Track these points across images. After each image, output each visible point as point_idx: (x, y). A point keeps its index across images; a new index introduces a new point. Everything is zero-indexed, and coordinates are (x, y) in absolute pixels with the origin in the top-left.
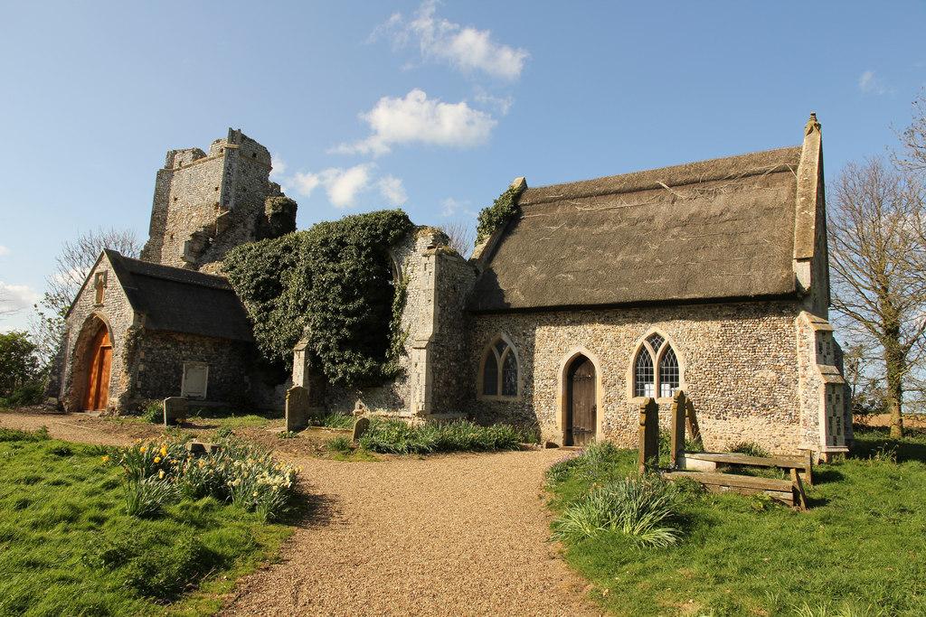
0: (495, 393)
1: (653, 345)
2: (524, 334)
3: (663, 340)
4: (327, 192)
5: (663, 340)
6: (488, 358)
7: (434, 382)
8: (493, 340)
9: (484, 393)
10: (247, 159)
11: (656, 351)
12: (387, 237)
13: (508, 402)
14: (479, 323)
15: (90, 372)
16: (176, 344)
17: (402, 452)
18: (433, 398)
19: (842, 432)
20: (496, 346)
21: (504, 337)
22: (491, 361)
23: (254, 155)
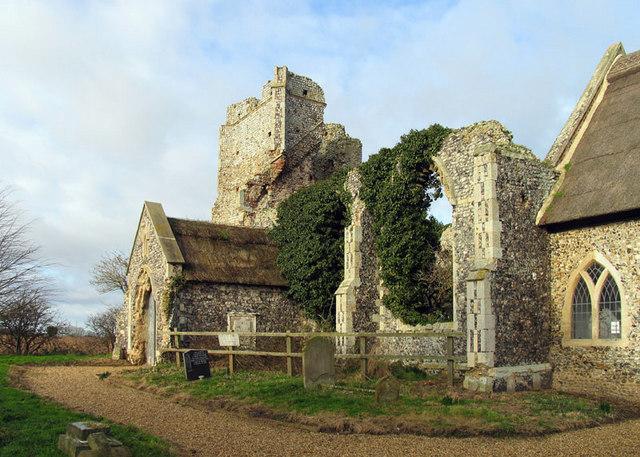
0: (587, 335)
1: (592, 276)
2: (629, 251)
3: (603, 269)
4: (371, 120)
5: (603, 269)
6: (576, 292)
7: (497, 325)
8: (583, 263)
9: (574, 336)
10: (299, 95)
11: (595, 282)
12: (418, 159)
13: (607, 349)
14: (561, 242)
15: (338, 234)
16: (218, 296)
17: (172, 300)
18: (497, 346)
19: (468, 331)
20: (589, 271)
21: (600, 258)
22: (581, 290)
23: (305, 92)
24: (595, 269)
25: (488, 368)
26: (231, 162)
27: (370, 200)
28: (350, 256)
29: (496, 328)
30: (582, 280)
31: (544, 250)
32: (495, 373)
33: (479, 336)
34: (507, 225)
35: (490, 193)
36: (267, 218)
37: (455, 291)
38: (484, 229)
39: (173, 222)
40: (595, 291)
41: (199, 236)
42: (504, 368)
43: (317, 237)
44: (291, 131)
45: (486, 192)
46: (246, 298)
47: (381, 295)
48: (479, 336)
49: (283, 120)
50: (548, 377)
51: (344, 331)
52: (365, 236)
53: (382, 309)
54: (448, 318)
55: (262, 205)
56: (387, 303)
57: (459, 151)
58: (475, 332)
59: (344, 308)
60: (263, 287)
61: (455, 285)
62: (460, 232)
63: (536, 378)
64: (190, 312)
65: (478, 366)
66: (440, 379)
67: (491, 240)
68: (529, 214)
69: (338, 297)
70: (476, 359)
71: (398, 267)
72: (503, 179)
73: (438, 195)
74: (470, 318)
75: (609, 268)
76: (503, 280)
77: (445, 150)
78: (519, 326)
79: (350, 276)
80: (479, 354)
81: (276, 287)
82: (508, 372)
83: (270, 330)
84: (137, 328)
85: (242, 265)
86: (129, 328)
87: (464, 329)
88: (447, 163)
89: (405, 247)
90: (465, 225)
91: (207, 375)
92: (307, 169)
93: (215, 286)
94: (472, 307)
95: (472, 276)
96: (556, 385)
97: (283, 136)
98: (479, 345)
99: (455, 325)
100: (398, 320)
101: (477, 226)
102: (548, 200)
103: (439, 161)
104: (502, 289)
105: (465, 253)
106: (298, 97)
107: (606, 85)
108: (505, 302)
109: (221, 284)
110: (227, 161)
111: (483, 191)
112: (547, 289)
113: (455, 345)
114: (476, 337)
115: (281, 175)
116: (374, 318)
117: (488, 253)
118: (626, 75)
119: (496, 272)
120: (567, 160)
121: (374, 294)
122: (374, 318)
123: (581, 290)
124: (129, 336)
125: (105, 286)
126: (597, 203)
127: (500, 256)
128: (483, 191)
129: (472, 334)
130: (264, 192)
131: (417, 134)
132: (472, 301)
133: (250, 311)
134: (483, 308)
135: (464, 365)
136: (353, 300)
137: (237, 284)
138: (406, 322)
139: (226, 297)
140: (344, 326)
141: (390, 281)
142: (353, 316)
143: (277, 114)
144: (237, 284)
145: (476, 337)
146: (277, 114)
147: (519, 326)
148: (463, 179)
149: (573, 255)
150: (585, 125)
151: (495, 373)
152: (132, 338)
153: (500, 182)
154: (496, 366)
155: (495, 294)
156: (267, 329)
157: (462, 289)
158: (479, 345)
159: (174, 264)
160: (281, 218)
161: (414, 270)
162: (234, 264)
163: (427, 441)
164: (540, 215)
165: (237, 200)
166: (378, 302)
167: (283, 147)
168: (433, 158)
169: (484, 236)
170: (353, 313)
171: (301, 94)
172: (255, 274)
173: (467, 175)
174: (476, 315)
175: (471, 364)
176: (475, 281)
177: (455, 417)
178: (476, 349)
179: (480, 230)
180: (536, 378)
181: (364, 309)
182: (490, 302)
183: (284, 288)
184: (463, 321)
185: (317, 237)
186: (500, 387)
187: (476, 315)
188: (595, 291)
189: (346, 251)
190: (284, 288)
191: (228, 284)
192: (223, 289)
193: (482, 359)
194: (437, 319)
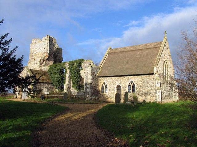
8: (103, 82)
16: (40, 85)
21: (105, 82)
22: (103, 86)
24: (104, 83)
27: (70, 69)
30: (155, 49)
31: (98, 80)
32: (90, 98)
34: (92, 77)
35: (90, 72)
36: (46, 68)
39: (30, 70)
40: (104, 86)
43: (59, 74)
44: (50, 48)
49: (48, 47)
50: (98, 98)
52: (69, 75)
53: (72, 88)
55: (43, 64)
56: (73, 87)
60: (49, 83)
63: (96, 99)
66: (82, 99)
68: (96, 75)
71: (75, 81)
73: (82, 69)
75: (106, 83)
78: (94, 91)
80: (89, 95)
81: (51, 83)
82: (92, 98)
85: (44, 79)
87: (86, 91)
89: (76, 78)
90: (86, 76)
91: (44, 99)
92: (52, 57)
96: (99, 100)
97: (48, 50)
102: (98, 72)
103: (82, 65)
107: (108, 54)
112: (98, 86)
113: (85, 94)
115: (49, 57)
116: (71, 89)
117: (90, 81)
118: (111, 53)
120: (101, 66)
121: (71, 85)
123: (103, 86)
126: (104, 74)
130: (44, 62)
136: (67, 86)
141: (73, 83)
147: (94, 91)
149: (102, 81)
150: (104, 61)
151: (90, 98)
153: (92, 71)
160: (49, 69)
161: (78, 81)
162: (43, 79)
163: (83, 105)
164: (97, 75)
167: (48, 53)
172: (47, 81)
177: (86, 102)
180: (96, 99)
181: (69, 88)
183: (52, 83)
184: (86, 90)
185: (59, 74)
186: (91, 100)
188: (104, 86)
189: (66, 78)
190: (52, 83)
191: (42, 83)
193: (89, 96)
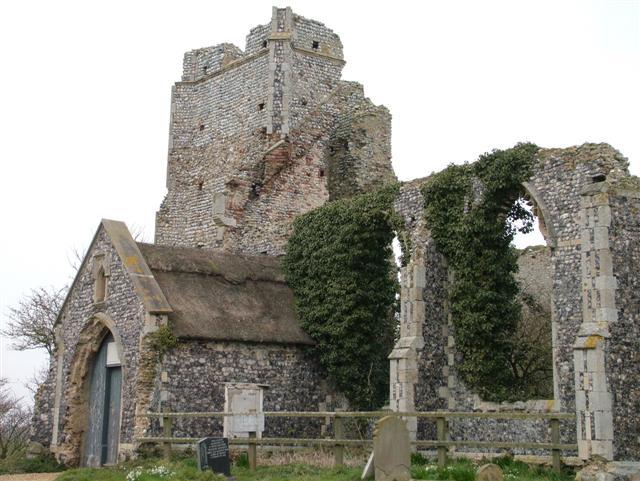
12: (507, 177)
16: (213, 358)
18: (616, 433)
23: (315, 45)
25: (605, 462)
26: (191, 141)
28: (409, 305)
29: (613, 410)
33: (592, 418)
35: (602, 242)
37: (555, 359)
38: (594, 285)
41: (182, 272)
42: (626, 463)
45: (596, 241)
46: (250, 362)
47: (451, 362)
48: (592, 418)
51: (403, 409)
54: (549, 396)
57: (559, 180)
58: (588, 414)
59: (402, 378)
61: (555, 351)
62: (560, 282)
64: (176, 383)
65: (593, 458)
67: (603, 299)
69: (393, 364)
70: (590, 449)
72: (617, 224)
74: (580, 396)
76: (620, 349)
77: (540, 176)
79: (408, 338)
83: (281, 409)
84: (72, 410)
86: (56, 411)
87: (571, 410)
88: (542, 194)
92: (316, 161)
93: (209, 345)
94: (582, 382)
95: (580, 342)
98: (593, 431)
99: (556, 405)
100: (476, 397)
101: (586, 282)
104: (619, 360)
105: (568, 309)
106: (306, 53)
108: (623, 377)
109: (217, 341)
110: (184, 139)
111: (592, 239)
114: (588, 420)
119: (610, 339)
121: (441, 359)
122: (442, 392)
124: (56, 422)
125: (22, 340)
127: (615, 319)
128: (592, 239)
129: (584, 416)
131: (498, 154)
132: (582, 374)
133: (253, 381)
134: (595, 383)
135: (571, 458)
136: (415, 367)
137: (239, 342)
138: (485, 399)
139: (223, 361)
140: (402, 403)
142: (415, 389)
143: (276, 81)
144: (239, 342)
145: (588, 420)
146: (276, 81)
148: (565, 215)
152: (62, 427)
153: (614, 229)
154: (617, 458)
155: (611, 366)
156: (278, 407)
157: (566, 356)
158: (583, 423)
159: (157, 314)
165: (218, 202)
166: (445, 370)
168: (525, 184)
169: (594, 294)
170: (415, 386)
171: (309, 47)
173: (569, 210)
174: (587, 392)
175: (583, 454)
176: (585, 349)
178: (589, 437)
179: (589, 287)
181: (429, 379)
182: (604, 378)
184: (569, 398)
187: (587, 392)
191: (227, 342)
192: (220, 348)
194: (537, 395)
